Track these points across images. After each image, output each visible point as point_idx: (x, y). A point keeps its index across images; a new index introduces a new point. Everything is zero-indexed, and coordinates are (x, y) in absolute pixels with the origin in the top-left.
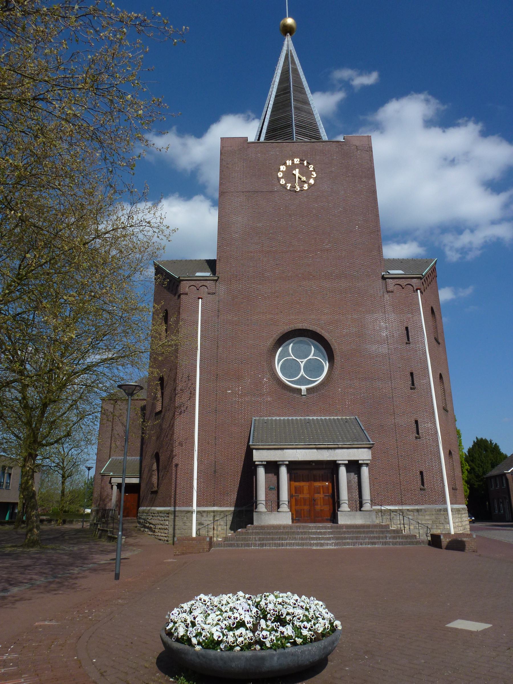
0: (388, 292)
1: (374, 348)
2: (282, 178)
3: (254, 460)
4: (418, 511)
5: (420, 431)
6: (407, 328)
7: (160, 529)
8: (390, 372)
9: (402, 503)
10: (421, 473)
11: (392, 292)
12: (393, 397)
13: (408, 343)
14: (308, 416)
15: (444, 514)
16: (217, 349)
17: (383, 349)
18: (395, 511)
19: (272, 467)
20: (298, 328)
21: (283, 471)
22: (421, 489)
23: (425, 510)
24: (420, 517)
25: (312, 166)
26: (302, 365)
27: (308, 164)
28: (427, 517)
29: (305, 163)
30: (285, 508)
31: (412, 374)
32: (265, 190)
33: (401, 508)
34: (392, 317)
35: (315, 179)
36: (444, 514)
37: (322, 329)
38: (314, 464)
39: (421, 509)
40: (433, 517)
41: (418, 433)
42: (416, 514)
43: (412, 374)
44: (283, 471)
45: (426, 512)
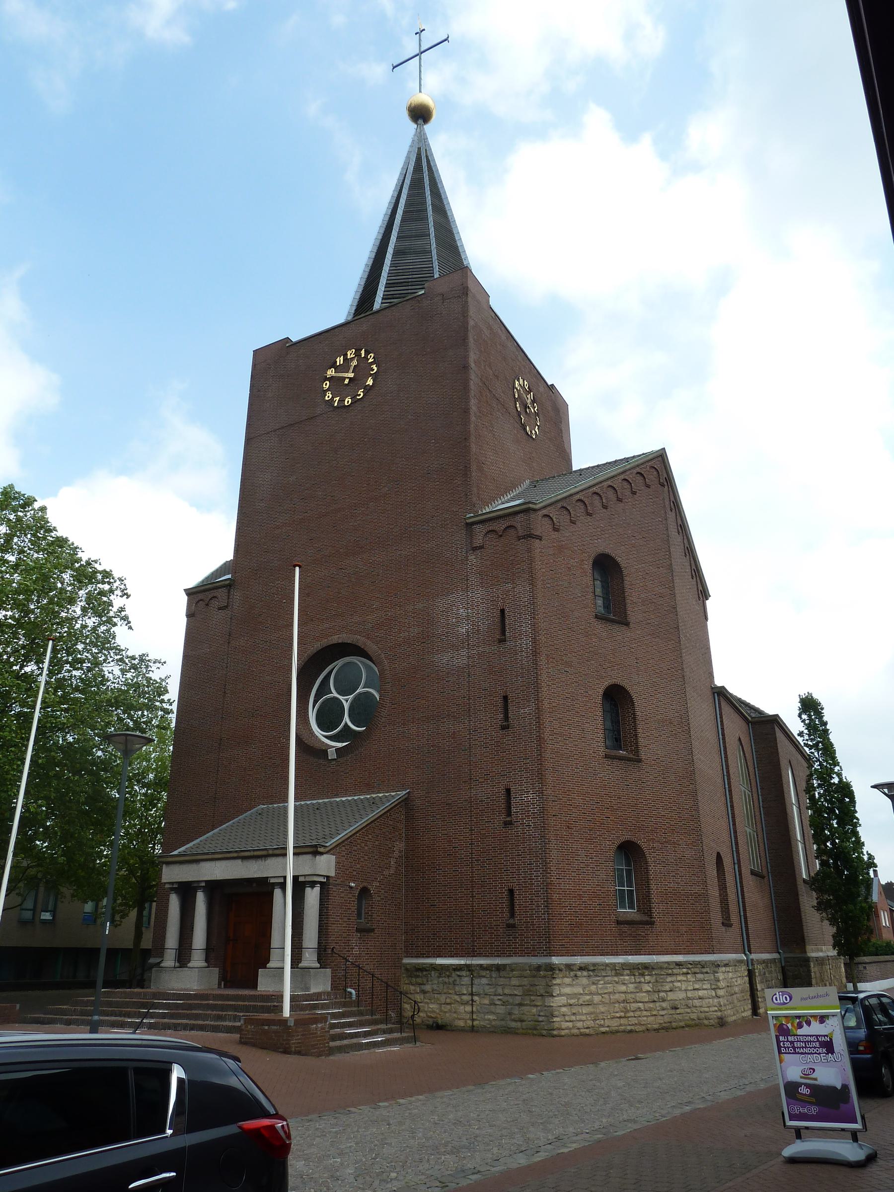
0: (474, 549)
1: (444, 659)
2: (328, 390)
3: (163, 881)
4: (499, 968)
5: (514, 810)
6: (502, 611)
7: (700, 998)
8: (469, 699)
9: (473, 954)
10: (511, 892)
11: (481, 547)
12: (470, 748)
13: (502, 641)
14: (337, 796)
15: (545, 977)
16: (224, 696)
17: (461, 659)
18: (458, 968)
19: (186, 891)
20: (335, 642)
21: (201, 899)
22: (509, 926)
23: (512, 968)
24: (502, 981)
25: (372, 355)
26: (346, 706)
27: (367, 353)
28: (515, 982)
29: (363, 352)
30: (198, 960)
31: (505, 698)
32: (305, 418)
33: (468, 962)
34: (478, 594)
35: (375, 377)
36: (545, 977)
37: (368, 638)
38: (254, 885)
39: (505, 965)
40: (525, 981)
41: (509, 814)
42: (494, 974)
43: (505, 698)
44: (201, 899)
45: (512, 970)
